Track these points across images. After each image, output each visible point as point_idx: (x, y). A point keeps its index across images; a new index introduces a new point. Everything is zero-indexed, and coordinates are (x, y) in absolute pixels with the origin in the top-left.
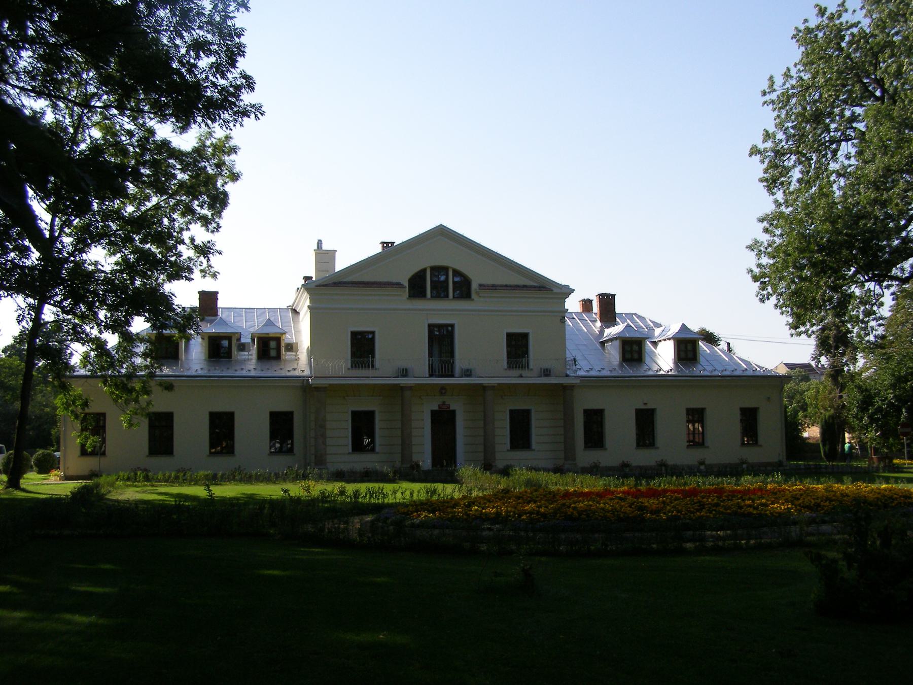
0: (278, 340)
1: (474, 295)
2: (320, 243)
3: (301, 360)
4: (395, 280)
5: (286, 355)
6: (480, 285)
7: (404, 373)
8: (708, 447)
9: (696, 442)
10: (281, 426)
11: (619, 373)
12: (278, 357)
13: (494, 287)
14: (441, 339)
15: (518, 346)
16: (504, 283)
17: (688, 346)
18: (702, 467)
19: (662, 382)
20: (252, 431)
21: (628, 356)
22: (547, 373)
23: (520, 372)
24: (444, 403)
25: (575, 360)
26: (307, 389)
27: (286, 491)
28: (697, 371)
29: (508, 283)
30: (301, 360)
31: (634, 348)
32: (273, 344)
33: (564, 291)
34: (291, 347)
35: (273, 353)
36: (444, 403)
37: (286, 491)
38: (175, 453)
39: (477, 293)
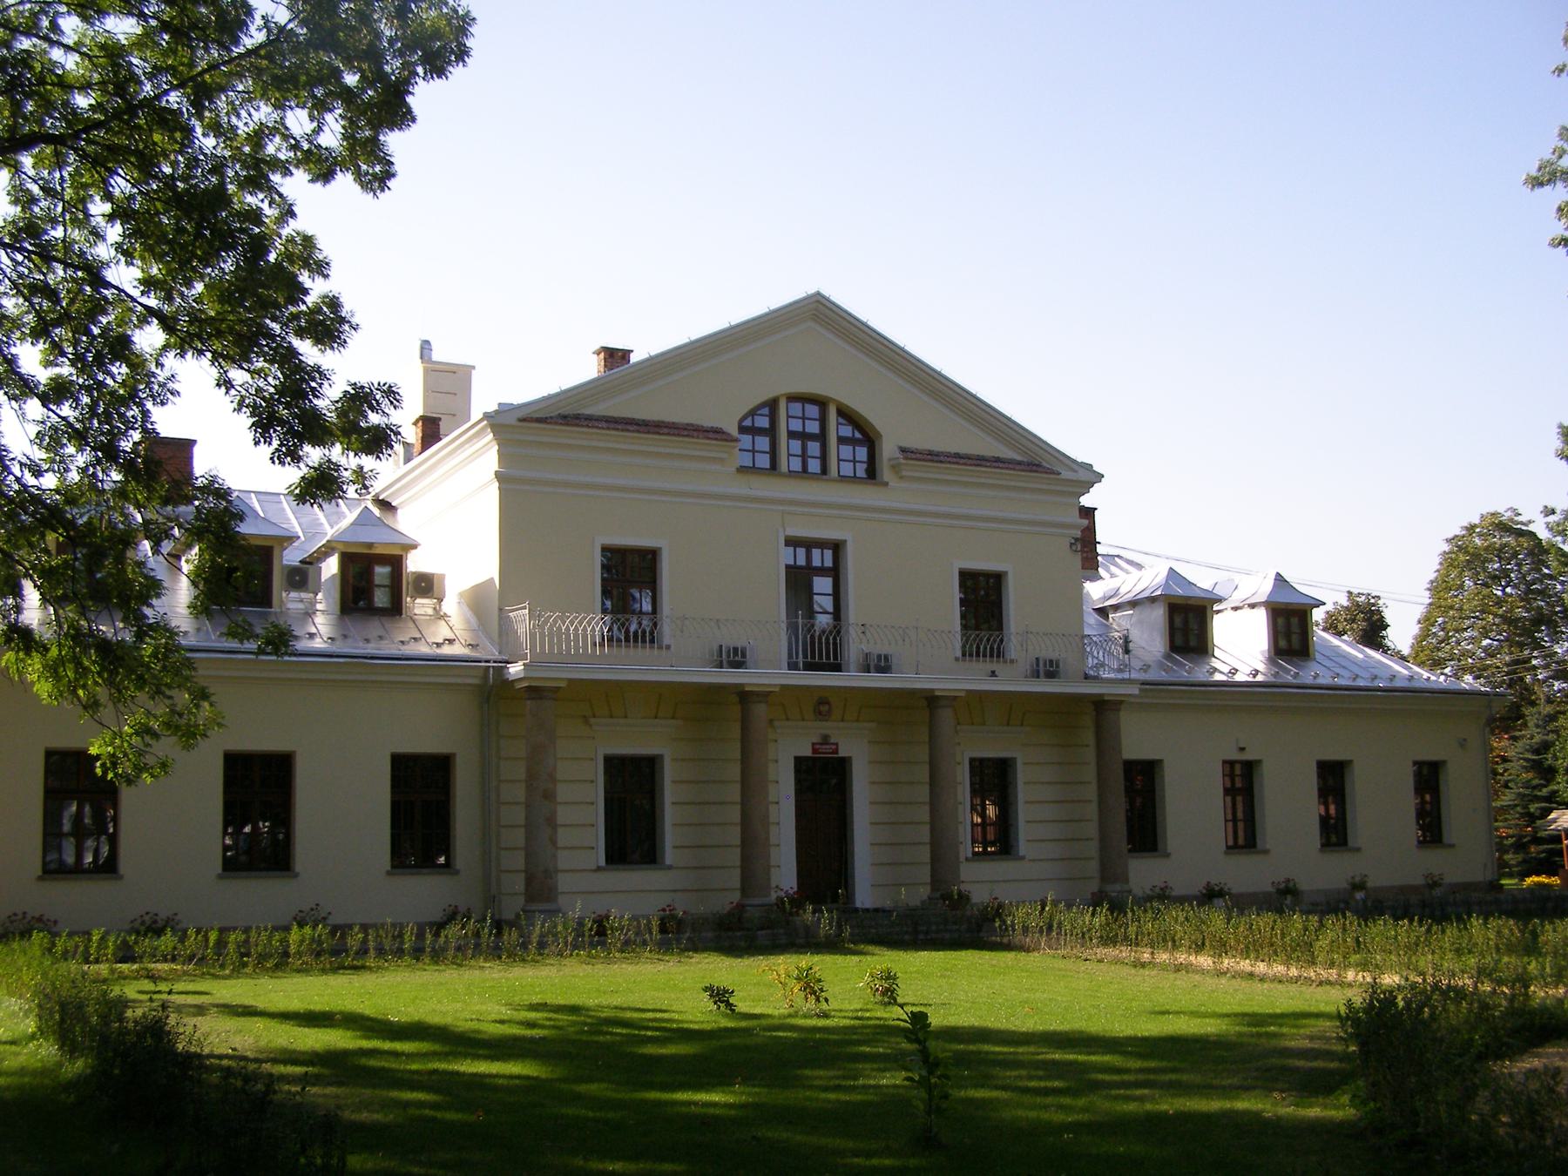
0: (396, 562)
1: (886, 473)
2: (426, 346)
3: (444, 628)
4: (707, 423)
5: (421, 607)
6: (903, 450)
7: (737, 658)
8: (1266, 852)
9: (1335, 833)
10: (421, 802)
11: (1163, 676)
12: (396, 609)
13: (932, 457)
14: (812, 573)
15: (983, 599)
16: (953, 450)
17: (1290, 622)
18: (1359, 895)
19: (1236, 696)
20: (340, 811)
21: (1179, 642)
22: (1051, 670)
23: (989, 666)
24: (825, 740)
25: (1127, 640)
26: (487, 691)
27: (720, 996)
28: (1314, 673)
29: (963, 450)
30: (444, 628)
31: (1188, 618)
32: (381, 572)
33: (1083, 476)
34: (427, 585)
35: (381, 598)
36: (825, 740)
37: (720, 996)
38: (299, 865)
39: (895, 468)
